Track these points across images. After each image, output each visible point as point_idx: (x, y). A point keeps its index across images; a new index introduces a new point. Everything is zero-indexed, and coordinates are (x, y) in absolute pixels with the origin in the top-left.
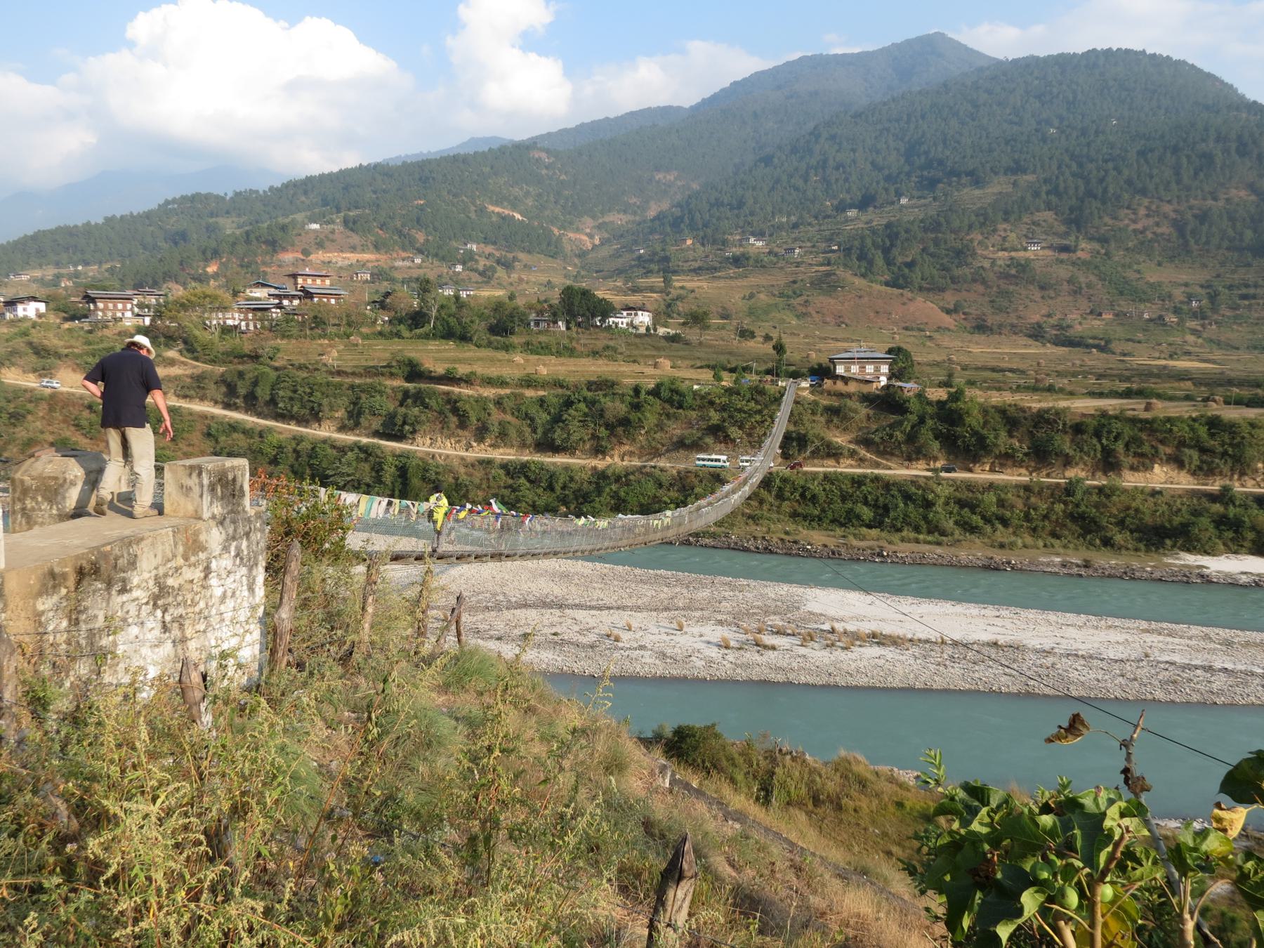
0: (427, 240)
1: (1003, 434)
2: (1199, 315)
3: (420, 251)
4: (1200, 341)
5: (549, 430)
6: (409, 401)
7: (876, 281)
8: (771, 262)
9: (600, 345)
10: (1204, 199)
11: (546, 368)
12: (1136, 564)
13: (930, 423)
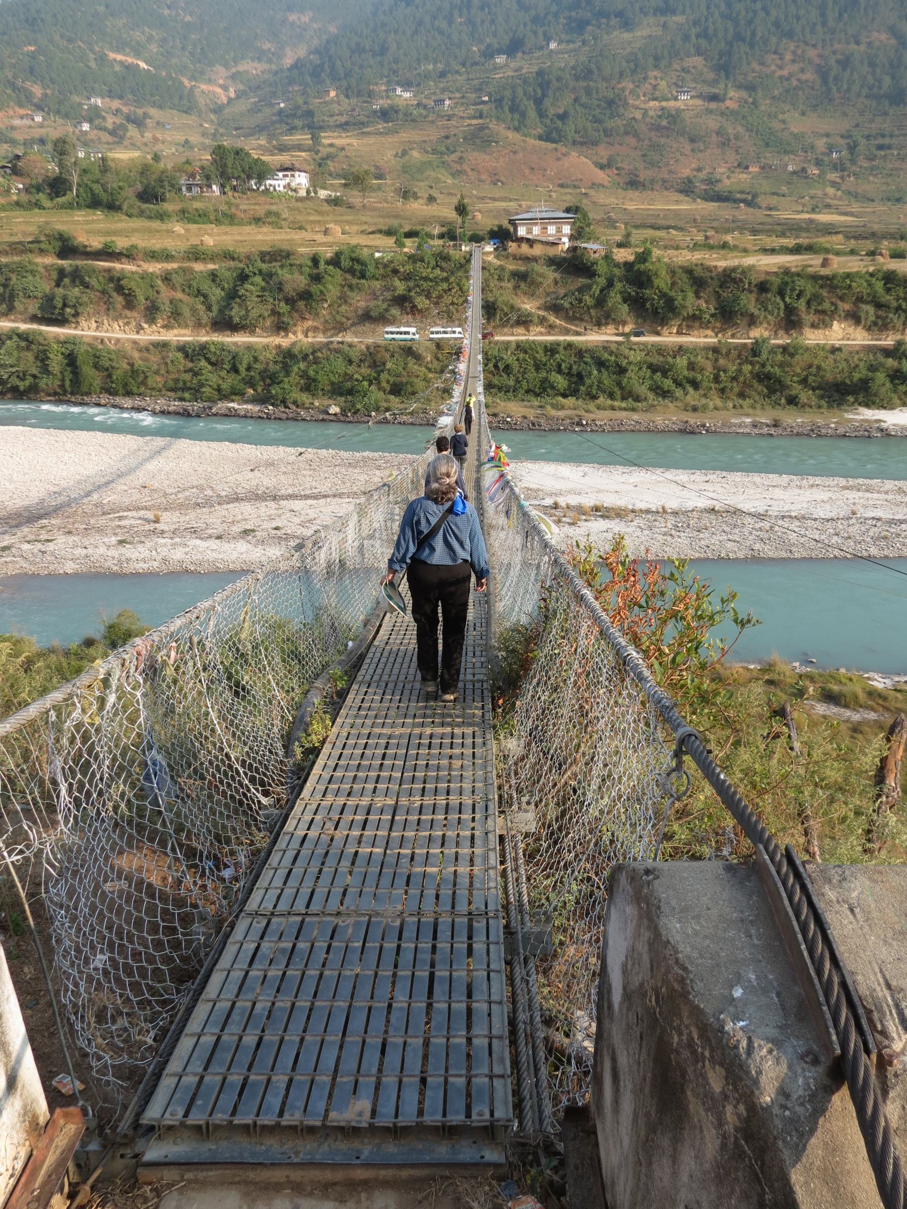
0: (46, 95)
1: (691, 295)
2: (839, 167)
3: (39, 107)
4: (839, 193)
5: (225, 307)
6: (66, 281)
7: (529, 135)
8: (421, 115)
9: (261, 211)
10: (848, 43)
11: (211, 238)
12: (820, 421)
13: (619, 286)
